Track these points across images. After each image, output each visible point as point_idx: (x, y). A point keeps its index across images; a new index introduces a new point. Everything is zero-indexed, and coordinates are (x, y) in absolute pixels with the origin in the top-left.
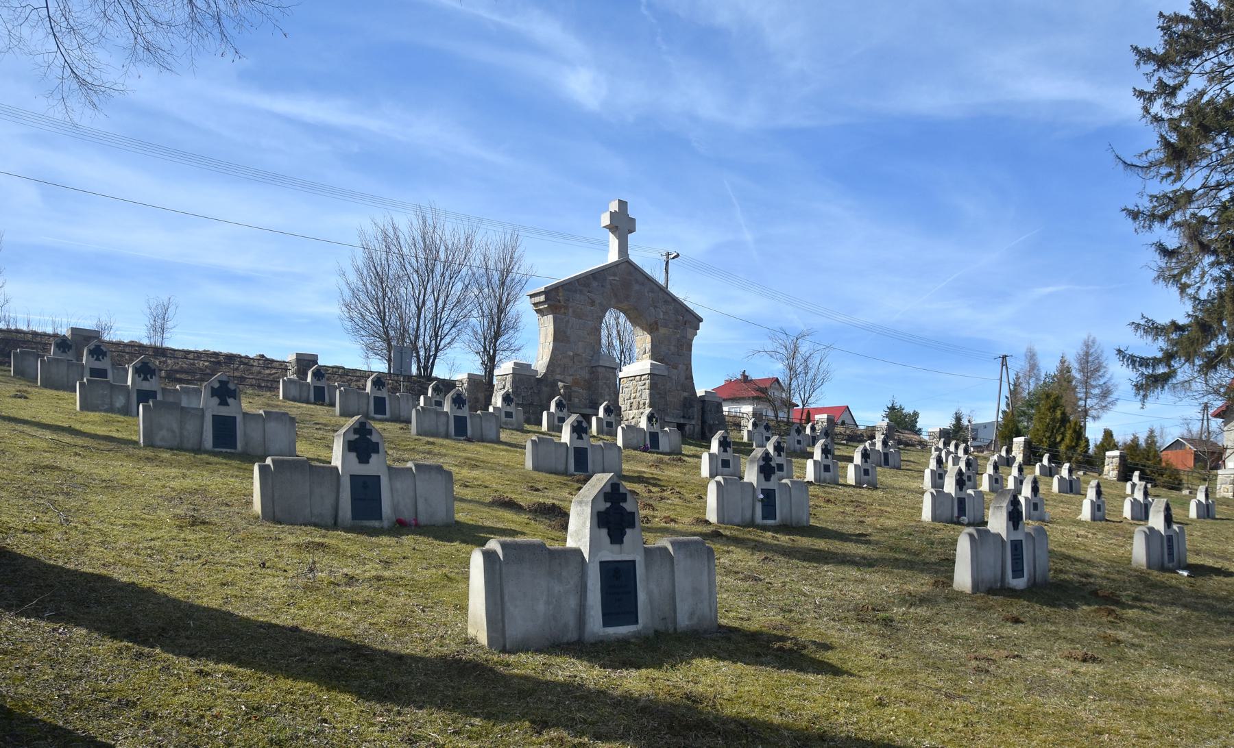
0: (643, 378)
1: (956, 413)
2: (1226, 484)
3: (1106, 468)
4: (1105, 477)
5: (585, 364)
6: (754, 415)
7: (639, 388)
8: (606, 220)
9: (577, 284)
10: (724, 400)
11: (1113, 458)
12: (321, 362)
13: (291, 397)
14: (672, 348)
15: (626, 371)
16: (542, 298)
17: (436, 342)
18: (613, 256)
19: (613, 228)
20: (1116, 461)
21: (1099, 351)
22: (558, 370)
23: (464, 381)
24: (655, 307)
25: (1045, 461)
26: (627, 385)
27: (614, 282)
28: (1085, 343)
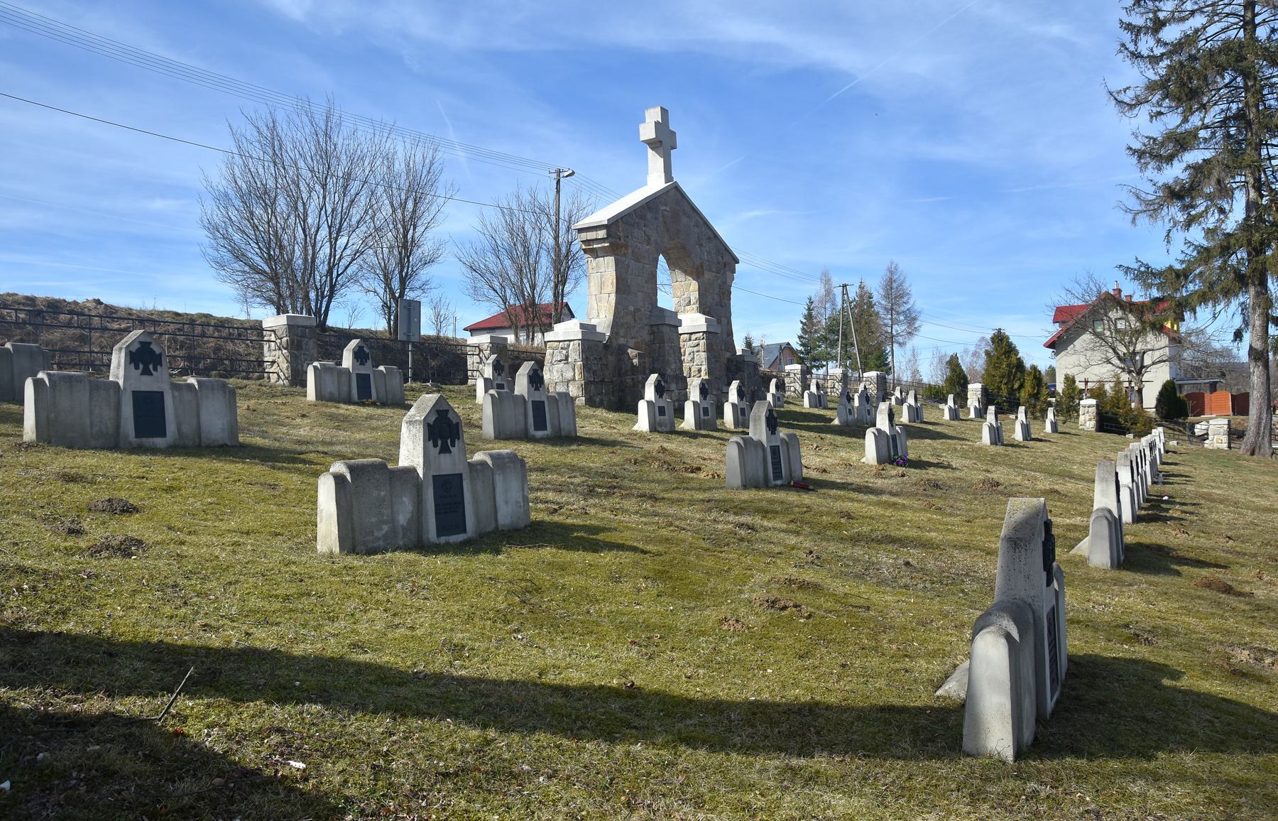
0: (693, 337)
1: (746, 338)
3: (1082, 418)
4: (1081, 427)
5: (645, 321)
11: (1089, 407)
13: (327, 396)
14: (716, 296)
16: (602, 234)
17: (331, 279)
18: (655, 183)
19: (654, 144)
20: (1094, 410)
21: (902, 278)
22: (622, 332)
24: (701, 245)
28: (888, 270)
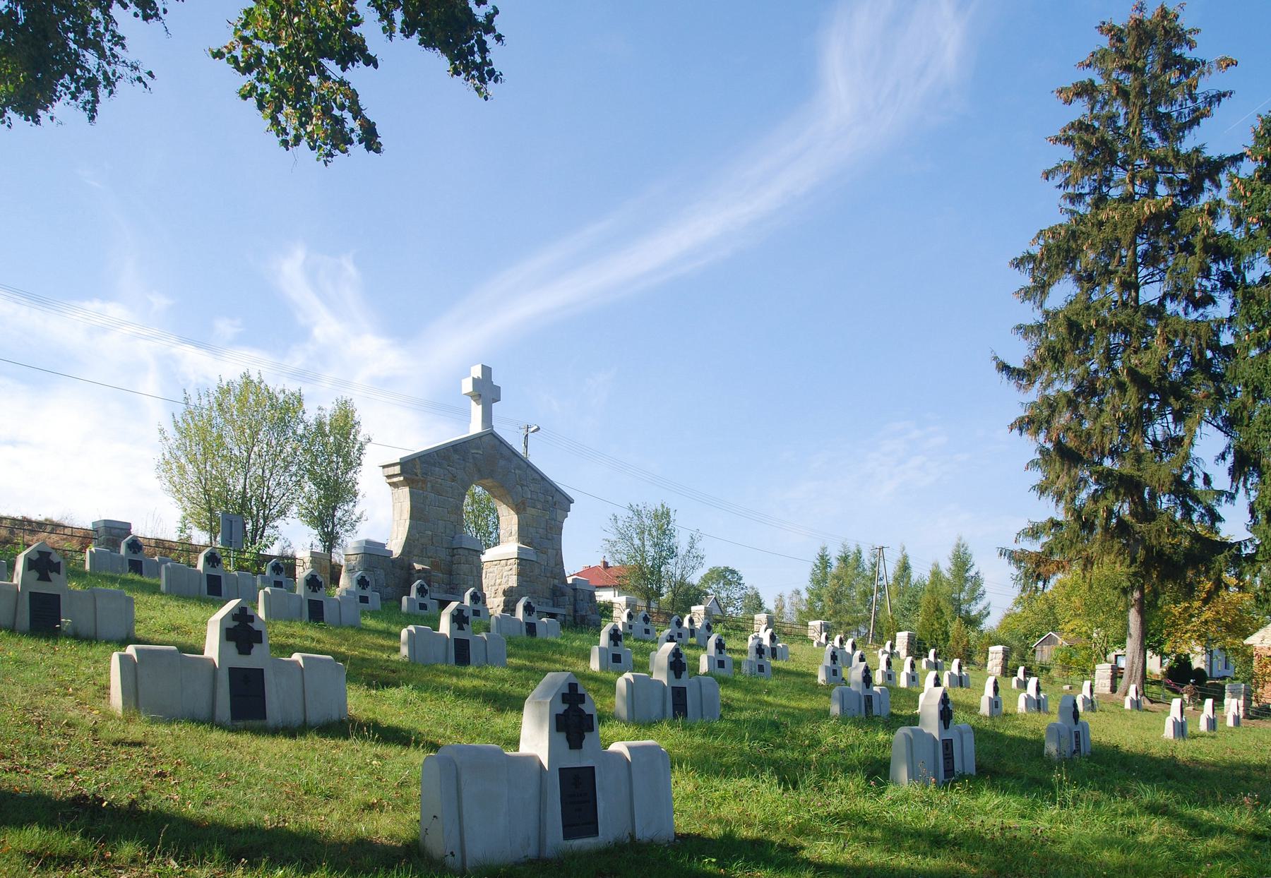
0: (509, 562)
2: (1103, 678)
6: (628, 605)
7: (505, 574)
8: (467, 386)
9: (436, 457)
10: (597, 587)
12: (134, 531)
15: (488, 555)
16: (397, 469)
23: (306, 560)
24: (522, 486)
25: (931, 657)
26: (491, 570)
27: (476, 456)
